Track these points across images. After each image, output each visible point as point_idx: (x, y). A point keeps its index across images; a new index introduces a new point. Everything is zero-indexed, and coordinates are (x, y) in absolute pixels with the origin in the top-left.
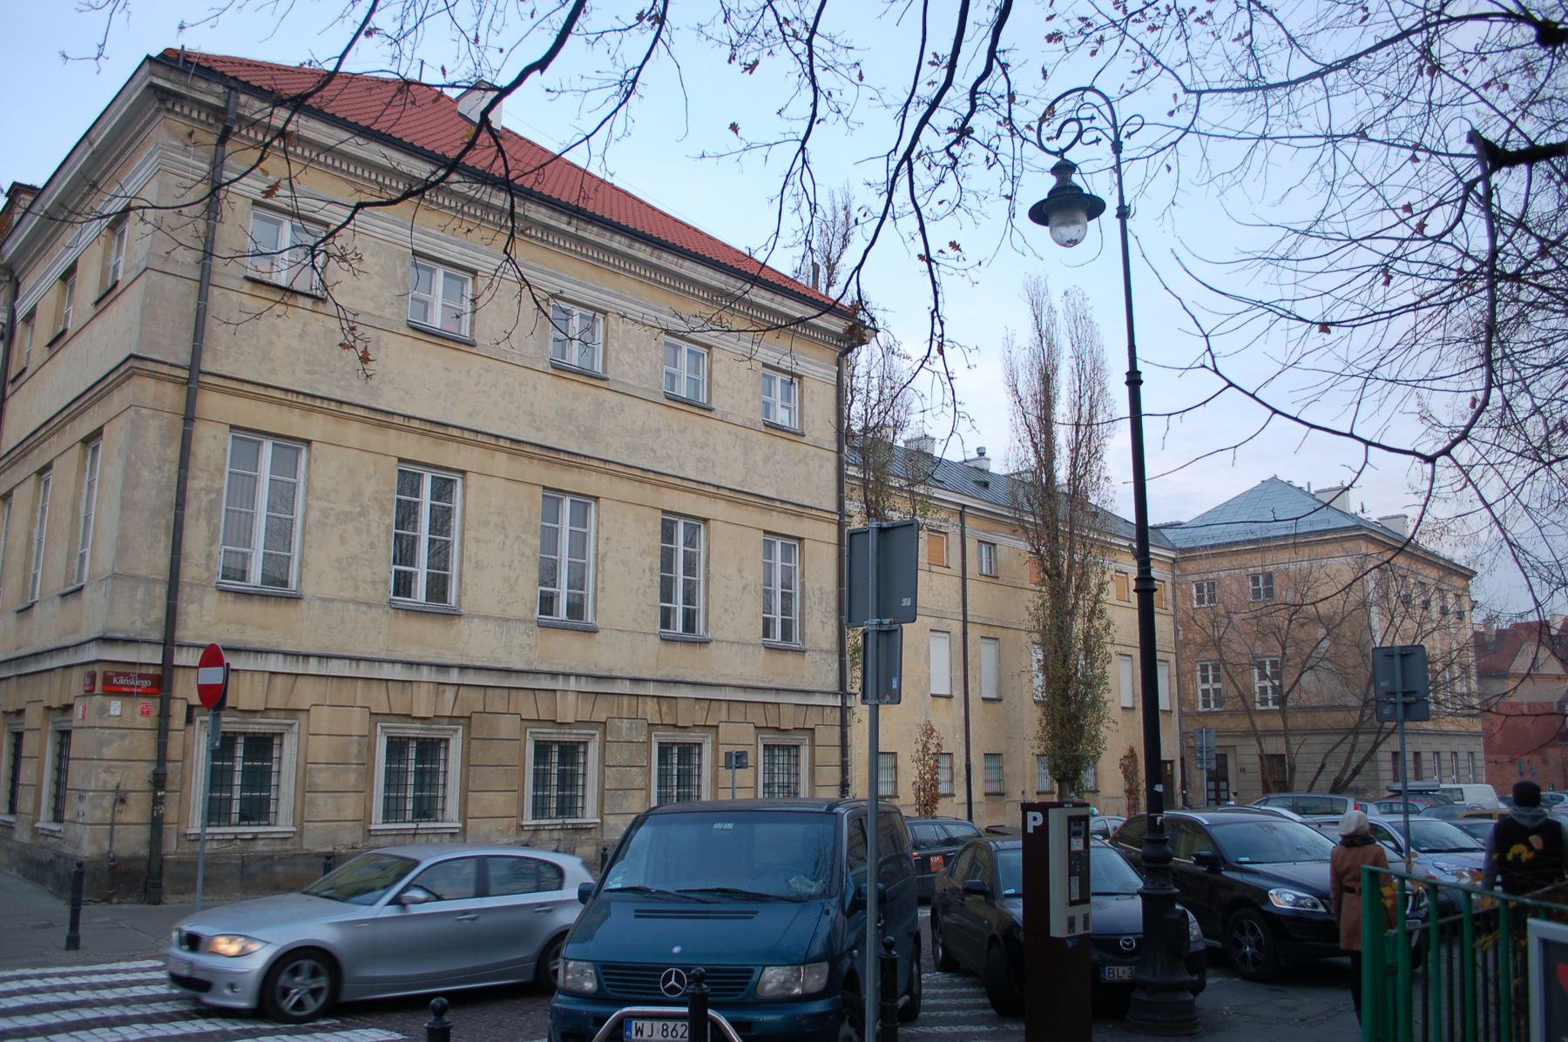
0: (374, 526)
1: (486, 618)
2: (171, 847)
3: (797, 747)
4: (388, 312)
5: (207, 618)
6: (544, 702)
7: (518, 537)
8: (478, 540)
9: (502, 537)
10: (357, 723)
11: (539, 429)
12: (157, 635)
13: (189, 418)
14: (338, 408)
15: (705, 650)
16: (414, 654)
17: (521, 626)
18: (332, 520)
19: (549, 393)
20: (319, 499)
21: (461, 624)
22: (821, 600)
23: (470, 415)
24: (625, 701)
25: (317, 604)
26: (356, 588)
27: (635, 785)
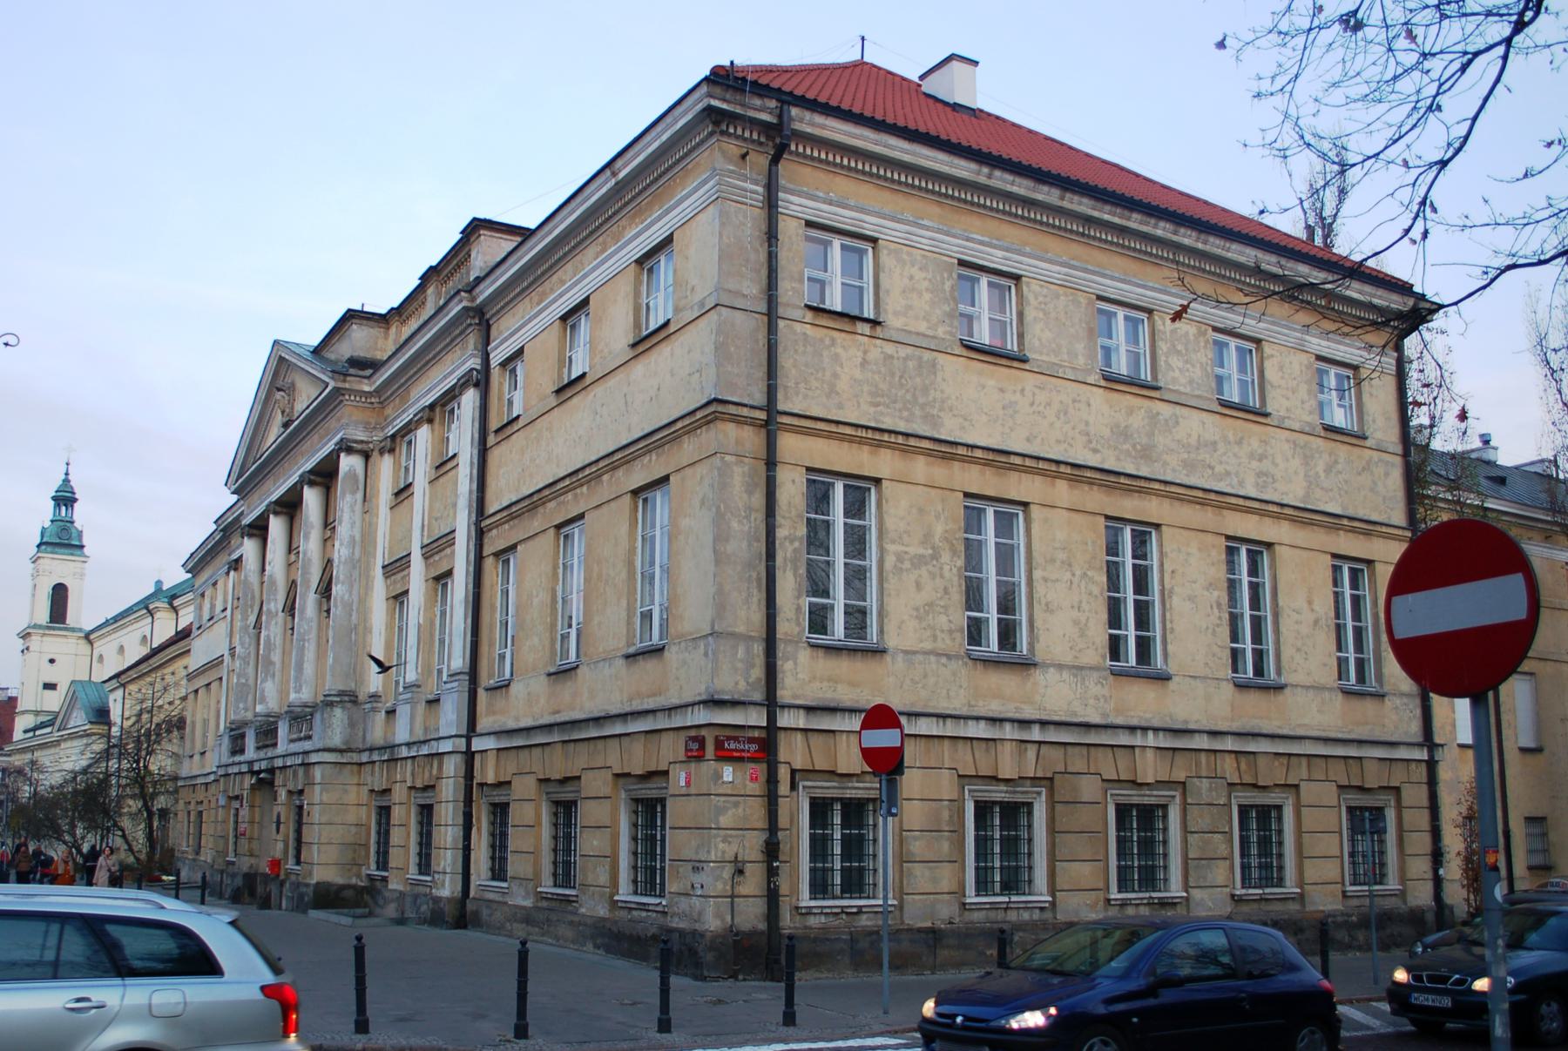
0: (946, 568)
1: (1060, 667)
5: (804, 675)
8: (1046, 580)
9: (1068, 575)
14: (903, 442)
16: (994, 708)
17: (1095, 675)
19: (1102, 409)
20: (893, 542)
21: (1037, 675)
26: (935, 638)
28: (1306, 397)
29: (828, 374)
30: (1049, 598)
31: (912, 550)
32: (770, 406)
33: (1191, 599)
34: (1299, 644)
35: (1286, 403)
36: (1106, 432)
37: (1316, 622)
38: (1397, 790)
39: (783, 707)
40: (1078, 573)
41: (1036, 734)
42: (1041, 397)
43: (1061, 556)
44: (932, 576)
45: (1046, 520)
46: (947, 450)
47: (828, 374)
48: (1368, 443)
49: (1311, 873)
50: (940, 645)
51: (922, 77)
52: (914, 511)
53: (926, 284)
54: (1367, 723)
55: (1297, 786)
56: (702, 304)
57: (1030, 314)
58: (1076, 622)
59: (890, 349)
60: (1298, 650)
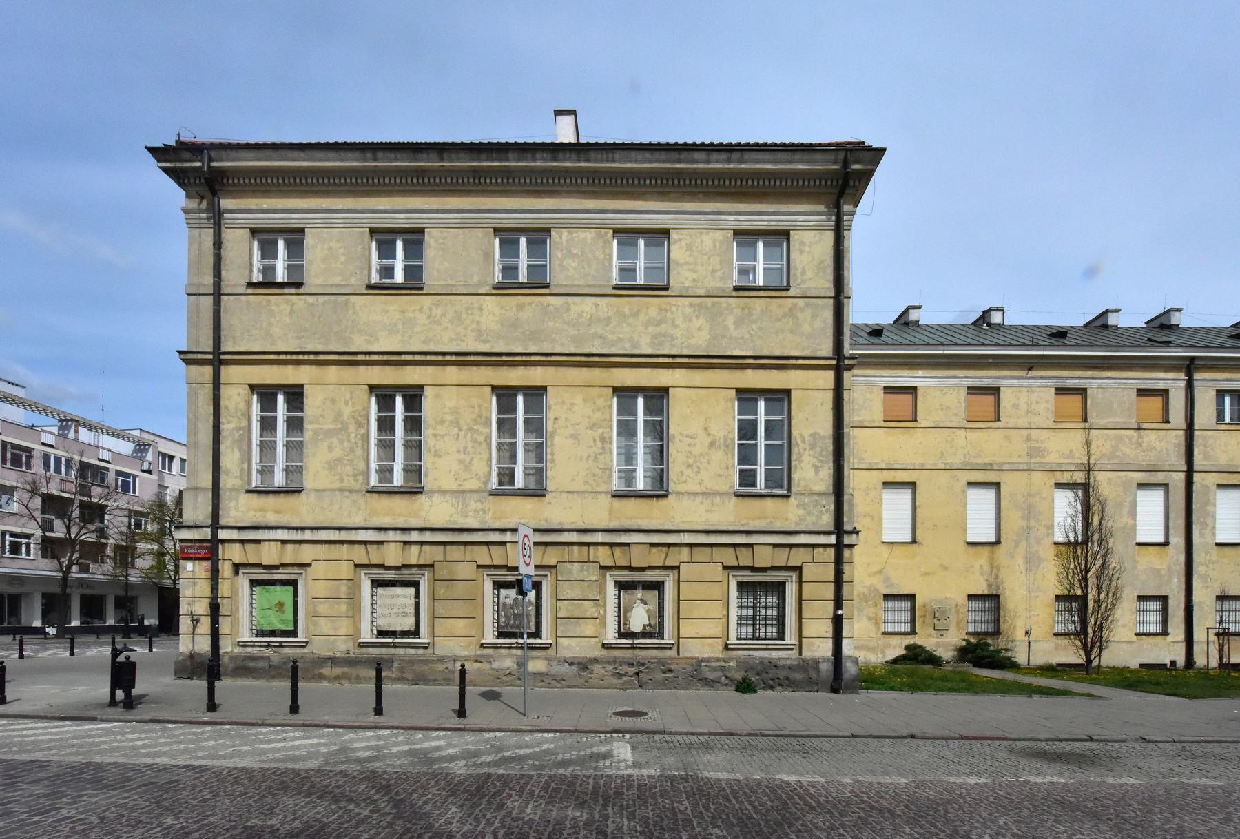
0: (352, 436)
1: (444, 492)
2: (226, 647)
3: (783, 584)
4: (353, 281)
5: (239, 509)
6: (743, 552)
7: (470, 429)
8: (435, 436)
9: (456, 430)
10: (345, 570)
11: (486, 341)
13: (217, 384)
14: (317, 359)
15: (663, 502)
16: (386, 521)
17: (475, 496)
18: (321, 436)
19: (494, 310)
20: (311, 423)
21: (422, 499)
22: (813, 446)
23: (424, 342)
24: (576, 548)
25: (313, 494)
26: (342, 480)
27: (588, 615)
28: (718, 267)
29: (265, 324)
30: (438, 447)
31: (326, 427)
32: (839, 372)
33: (574, 437)
34: (691, 461)
35: (691, 275)
36: (495, 327)
37: (712, 444)
38: (798, 569)
39: (222, 528)
40: (465, 428)
41: (415, 536)
42: (437, 312)
43: (449, 417)
44: (341, 442)
45: (437, 396)
46: (350, 359)
47: (265, 324)
48: (792, 293)
50: (345, 484)
52: (328, 402)
53: (342, 250)
54: (766, 518)
55: (678, 567)
58: (460, 462)
59: (311, 299)
60: (689, 466)
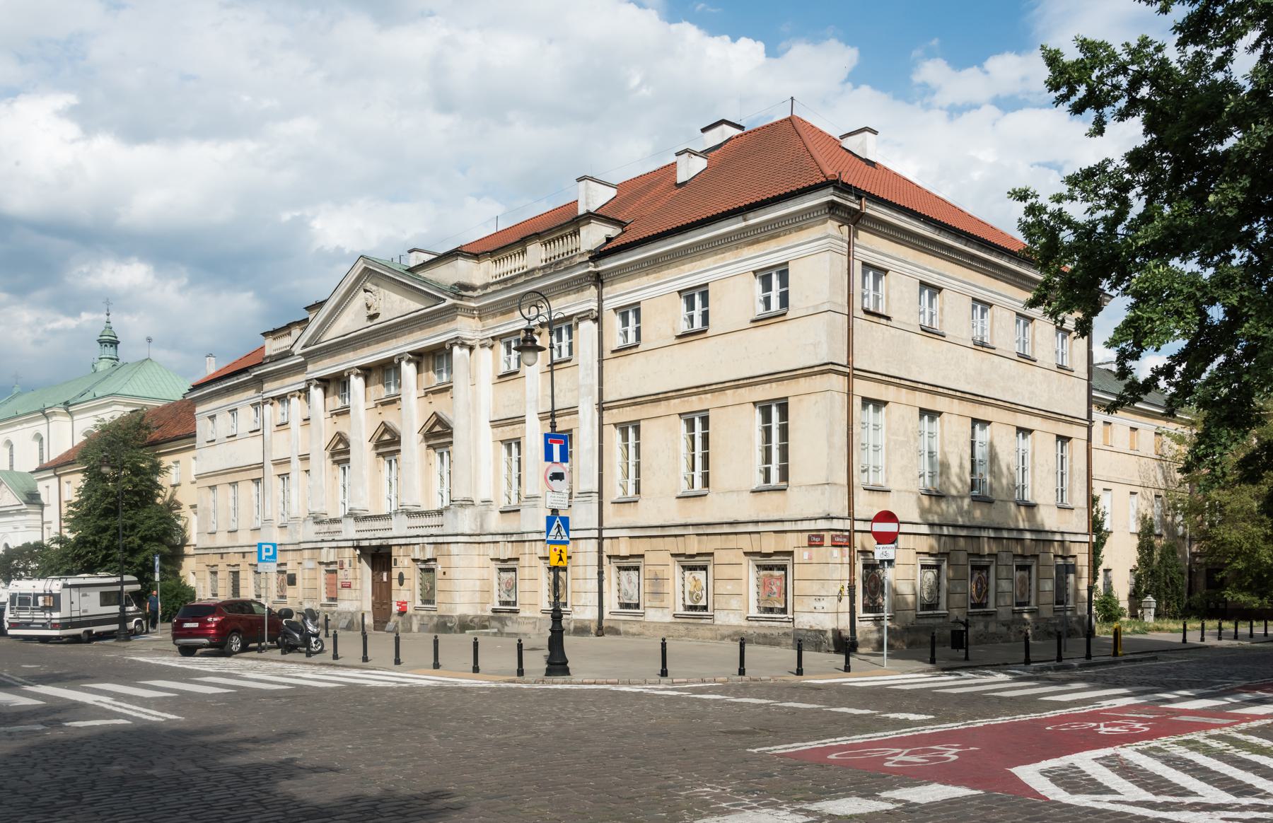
12: (846, 515)
46: (914, 386)
49: (1042, 600)
51: (842, 137)
56: (816, 307)
57: (946, 309)
